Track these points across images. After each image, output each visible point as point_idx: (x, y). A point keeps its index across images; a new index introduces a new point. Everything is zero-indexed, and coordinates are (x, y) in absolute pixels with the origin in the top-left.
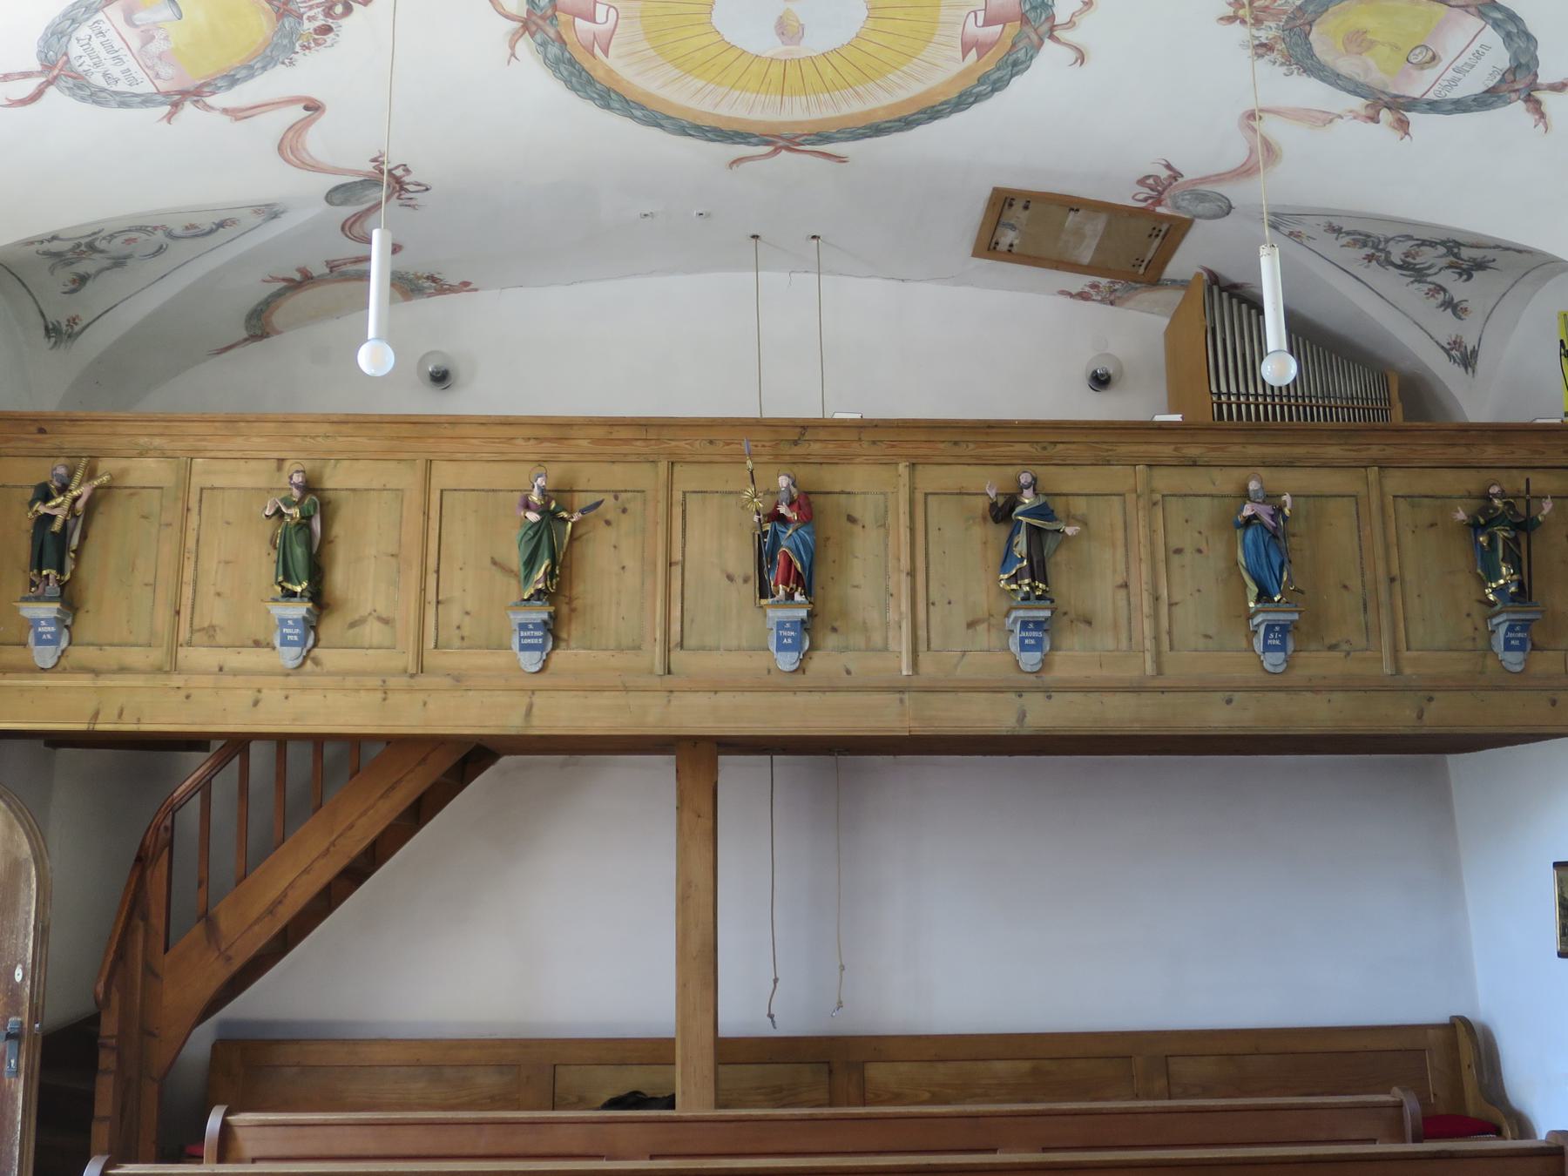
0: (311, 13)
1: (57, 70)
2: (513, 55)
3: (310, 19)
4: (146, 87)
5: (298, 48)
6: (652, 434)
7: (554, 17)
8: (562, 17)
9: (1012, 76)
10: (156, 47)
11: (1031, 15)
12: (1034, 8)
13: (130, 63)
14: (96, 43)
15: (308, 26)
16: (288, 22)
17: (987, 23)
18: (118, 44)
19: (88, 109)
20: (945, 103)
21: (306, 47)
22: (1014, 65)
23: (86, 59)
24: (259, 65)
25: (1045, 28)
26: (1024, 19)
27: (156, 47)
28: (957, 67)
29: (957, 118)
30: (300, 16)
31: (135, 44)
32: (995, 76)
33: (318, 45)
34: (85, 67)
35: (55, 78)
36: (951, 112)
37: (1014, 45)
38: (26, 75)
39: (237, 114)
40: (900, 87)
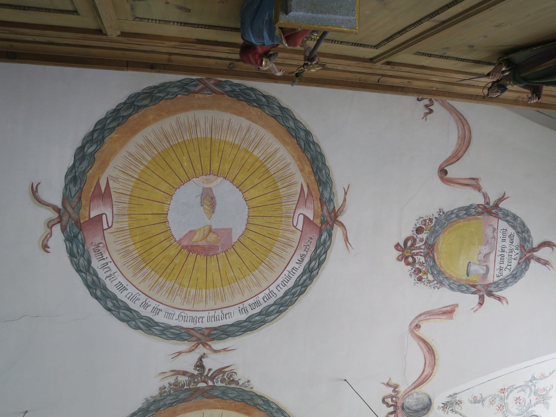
0: (421, 244)
1: (528, 254)
2: (346, 193)
3: (421, 240)
4: (503, 224)
5: (434, 220)
6: (374, 79)
7: (322, 223)
8: (318, 222)
9: (74, 165)
10: (485, 250)
11: (76, 230)
12: (76, 236)
13: (500, 244)
14: (504, 266)
15: (424, 236)
16: (431, 242)
17: (100, 217)
18: (498, 259)
19: (529, 225)
20: (113, 129)
21: (431, 220)
22: (75, 177)
23: (513, 257)
24: (453, 216)
25: (65, 218)
26: (77, 223)
27: (485, 250)
28: (110, 171)
29: (100, 113)
30: (426, 242)
31: (492, 256)
32: (85, 163)
33: (425, 221)
34: (517, 251)
35: (529, 252)
36: (106, 118)
37: (80, 198)
38: (538, 260)
39: (474, 184)
40: (142, 147)
